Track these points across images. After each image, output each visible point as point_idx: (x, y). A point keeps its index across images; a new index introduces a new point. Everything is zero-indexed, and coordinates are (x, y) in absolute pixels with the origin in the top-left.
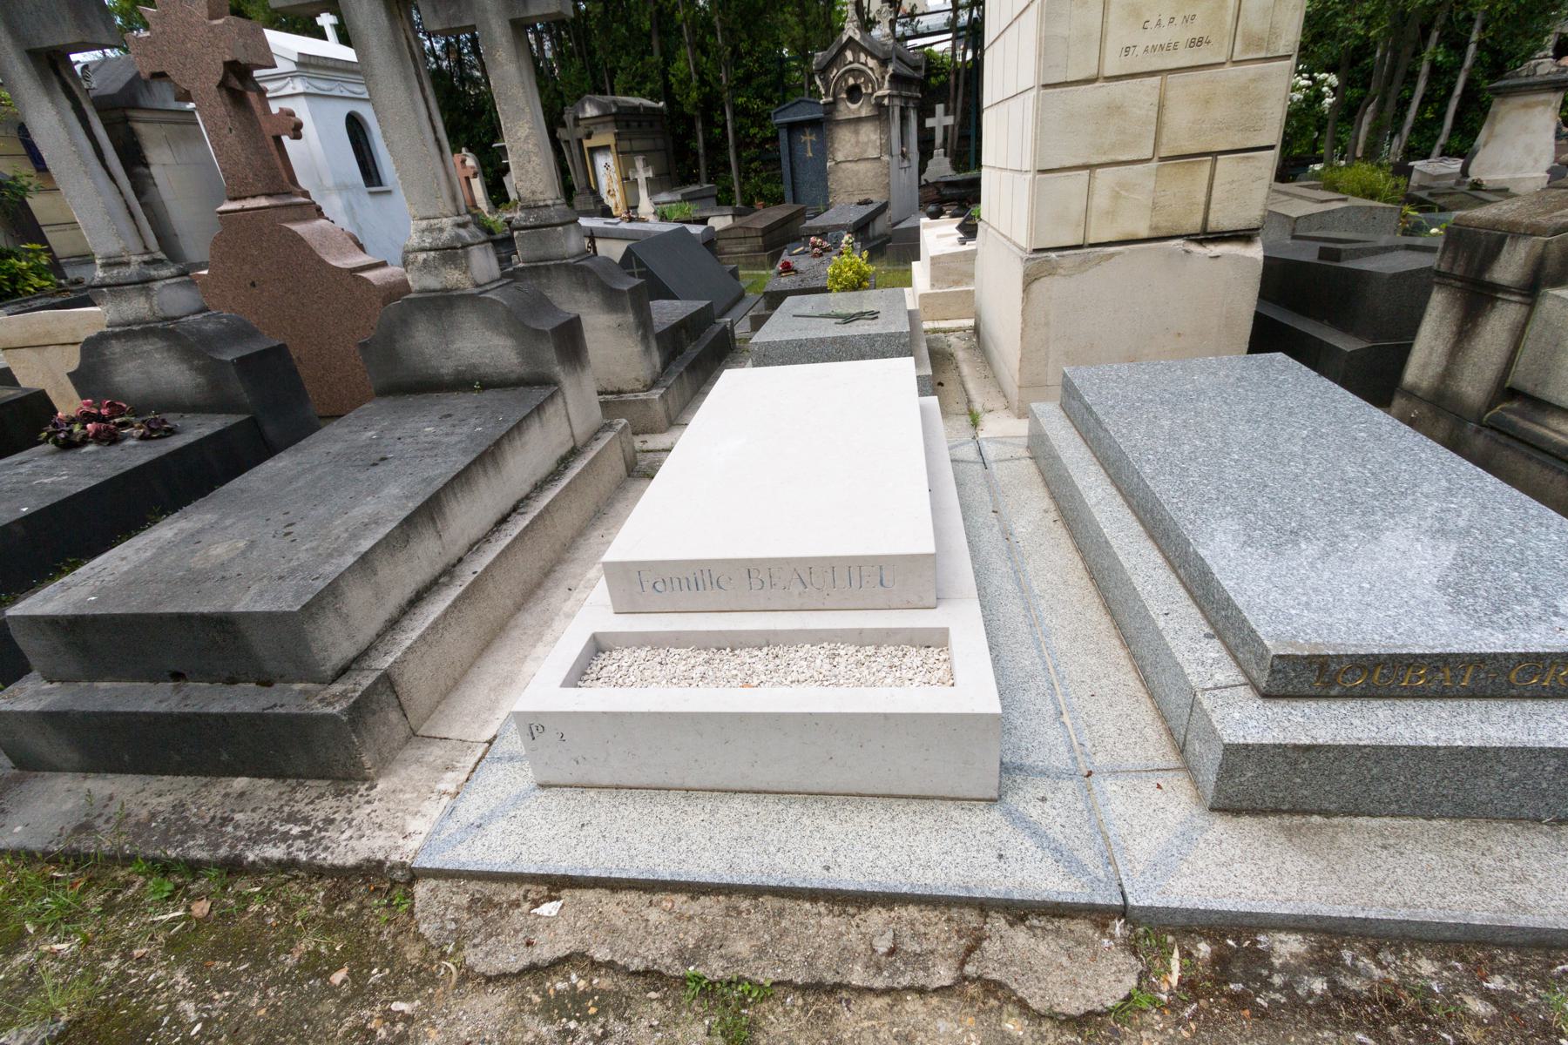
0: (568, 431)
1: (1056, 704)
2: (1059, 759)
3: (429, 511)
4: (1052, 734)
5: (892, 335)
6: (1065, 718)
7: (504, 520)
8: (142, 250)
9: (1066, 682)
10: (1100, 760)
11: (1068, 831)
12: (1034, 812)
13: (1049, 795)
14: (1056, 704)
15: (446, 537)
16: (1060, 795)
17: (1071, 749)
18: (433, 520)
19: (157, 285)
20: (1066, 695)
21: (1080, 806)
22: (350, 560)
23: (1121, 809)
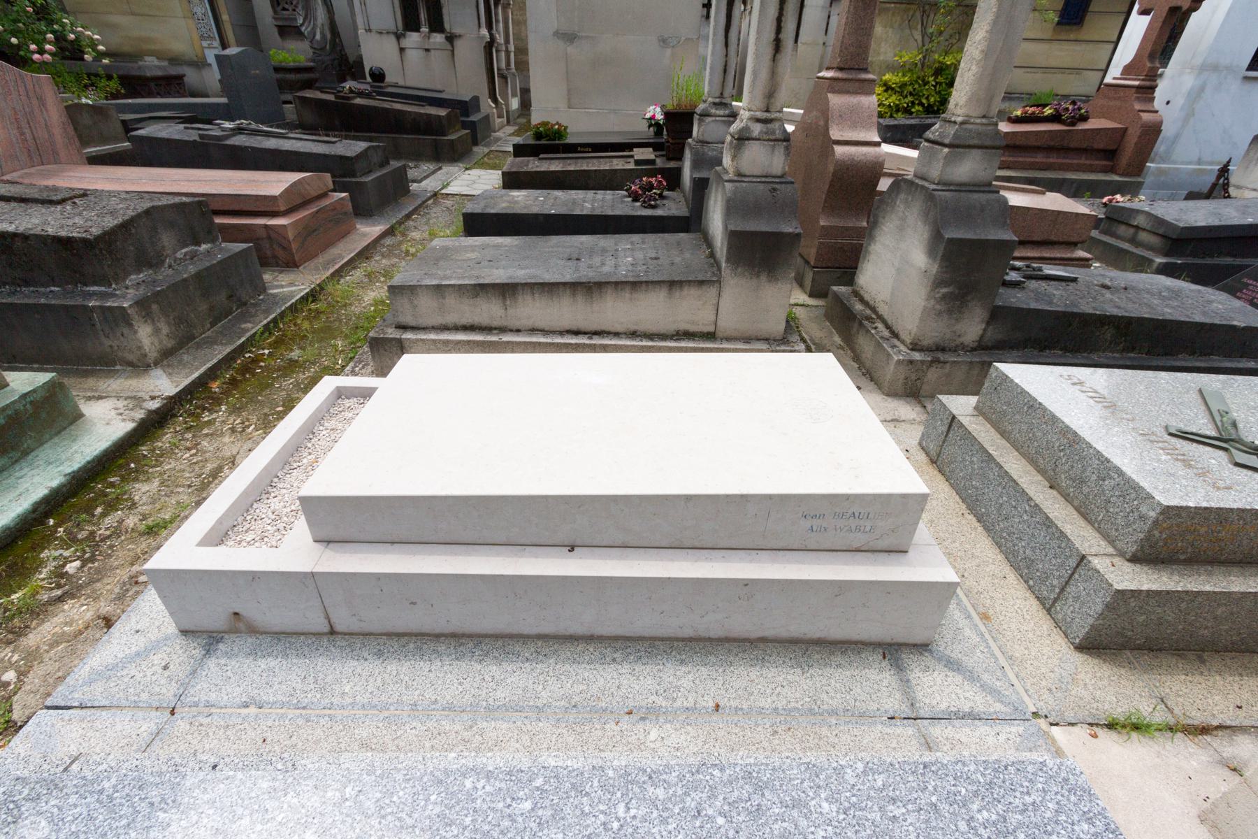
0: (713, 318)
1: (273, 705)
2: (202, 690)
3: (507, 291)
4: (235, 692)
5: (1137, 488)
6: (252, 710)
7: (577, 333)
8: (718, 94)
9: (300, 722)
10: (181, 725)
11: (126, 680)
12: (158, 659)
13: (167, 673)
14: (273, 705)
15: (511, 311)
16: (163, 681)
17: (209, 705)
18: (504, 298)
19: (709, 119)
20: (282, 716)
21: (144, 696)
22: (435, 282)
23: (119, 727)
